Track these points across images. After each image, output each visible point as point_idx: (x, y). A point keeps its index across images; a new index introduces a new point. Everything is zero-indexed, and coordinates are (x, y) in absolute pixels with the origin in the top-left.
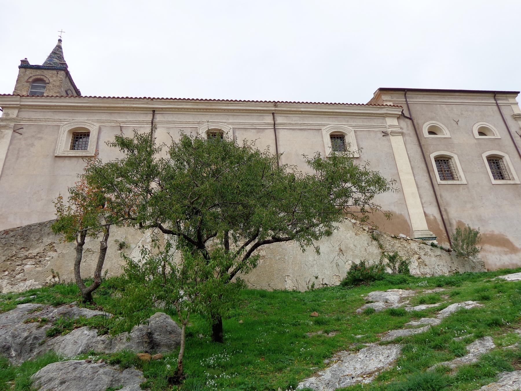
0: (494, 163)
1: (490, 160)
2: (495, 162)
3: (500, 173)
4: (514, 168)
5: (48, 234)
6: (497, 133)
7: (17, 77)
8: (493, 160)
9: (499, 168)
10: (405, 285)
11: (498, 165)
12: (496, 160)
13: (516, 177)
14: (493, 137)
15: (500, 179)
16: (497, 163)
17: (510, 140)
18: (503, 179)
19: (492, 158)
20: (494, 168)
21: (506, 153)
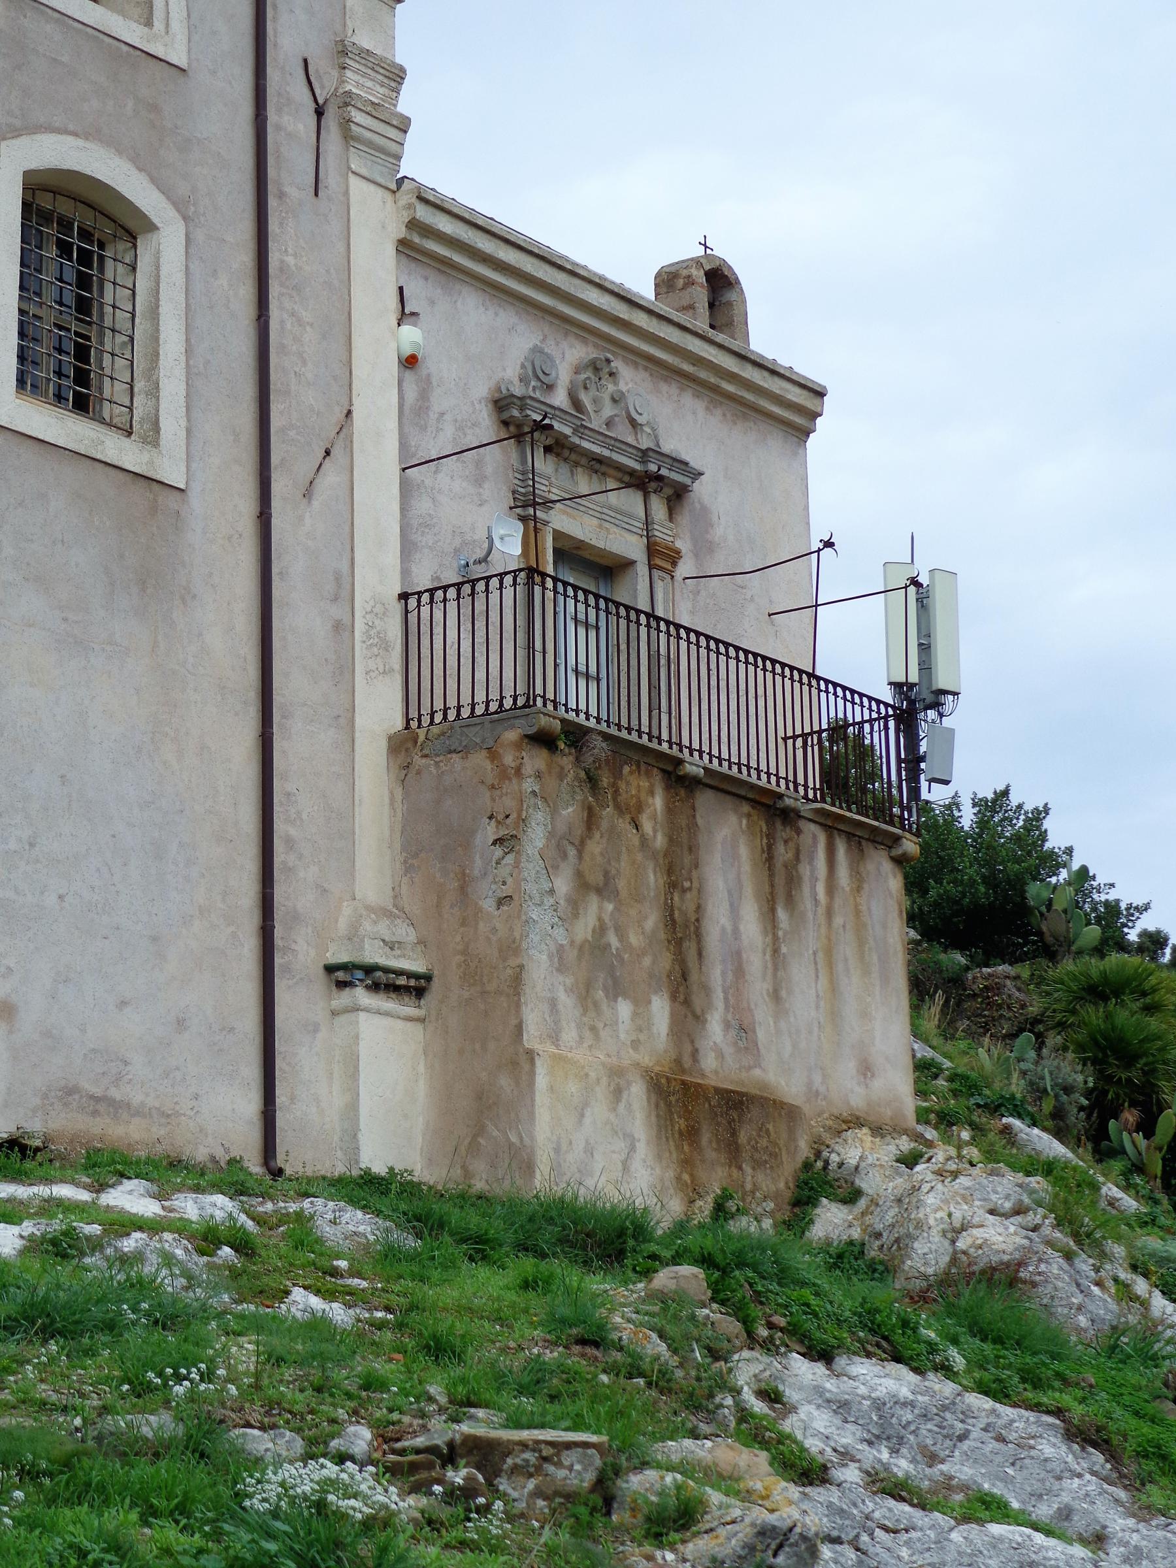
0: (64, 249)
1: (46, 217)
2: (74, 233)
3: (82, 353)
4: (189, 352)
5: (1139, 1168)
6: (178, 26)
7: (16, 269)
8: (65, 225)
9: (83, 307)
10: (375, 1200)
11: (84, 282)
12: (85, 235)
13: (172, 426)
14: (130, 31)
15: (59, 398)
16: (85, 258)
17: (246, 110)
18: (81, 405)
19: (64, 207)
20: (50, 295)
21: (180, 205)
